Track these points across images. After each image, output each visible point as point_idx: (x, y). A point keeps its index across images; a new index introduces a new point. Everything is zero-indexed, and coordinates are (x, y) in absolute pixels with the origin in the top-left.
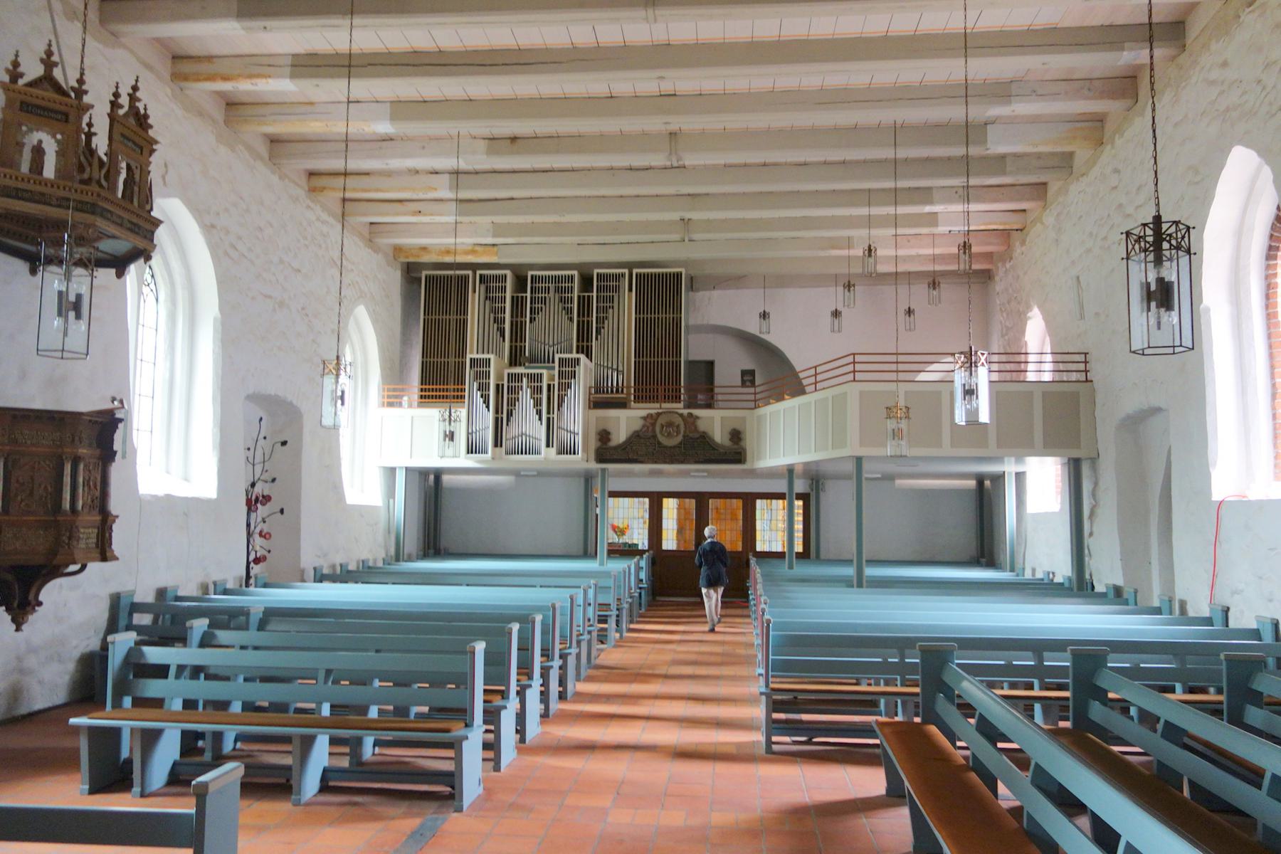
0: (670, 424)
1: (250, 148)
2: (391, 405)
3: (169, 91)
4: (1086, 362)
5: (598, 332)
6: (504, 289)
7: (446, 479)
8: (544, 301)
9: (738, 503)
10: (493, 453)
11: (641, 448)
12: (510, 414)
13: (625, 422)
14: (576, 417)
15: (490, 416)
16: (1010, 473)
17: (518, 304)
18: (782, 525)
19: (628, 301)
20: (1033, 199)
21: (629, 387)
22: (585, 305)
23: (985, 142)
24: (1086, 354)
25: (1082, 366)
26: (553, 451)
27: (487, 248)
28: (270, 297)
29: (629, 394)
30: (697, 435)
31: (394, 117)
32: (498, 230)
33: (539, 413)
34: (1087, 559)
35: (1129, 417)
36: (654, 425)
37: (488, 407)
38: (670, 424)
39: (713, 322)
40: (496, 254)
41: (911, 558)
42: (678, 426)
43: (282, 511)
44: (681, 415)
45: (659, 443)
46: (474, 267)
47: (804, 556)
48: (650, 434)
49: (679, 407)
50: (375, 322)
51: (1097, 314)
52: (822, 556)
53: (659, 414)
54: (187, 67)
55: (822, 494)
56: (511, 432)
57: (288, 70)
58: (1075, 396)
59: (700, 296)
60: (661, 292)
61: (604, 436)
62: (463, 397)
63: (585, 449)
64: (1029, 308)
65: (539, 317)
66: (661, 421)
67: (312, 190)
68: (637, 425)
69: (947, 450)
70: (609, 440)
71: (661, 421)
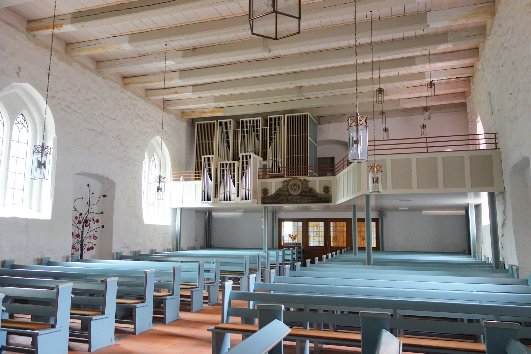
0: (295, 185)
1: (82, 65)
2: (174, 180)
3: (25, 37)
4: (496, 138)
6: (229, 128)
7: (214, 214)
8: (246, 132)
9: (322, 224)
10: (214, 200)
11: (282, 196)
13: (274, 185)
14: (250, 182)
16: (471, 205)
17: (236, 134)
18: (322, 234)
19: (283, 129)
20: (470, 57)
21: (284, 168)
22: (264, 131)
23: (426, 21)
24: (495, 134)
25: (493, 141)
27: (220, 109)
28: (93, 130)
29: (284, 172)
30: (307, 190)
31: (131, 41)
32: (217, 99)
33: (234, 181)
34: (501, 250)
35: (515, 167)
36: (287, 185)
37: (211, 179)
38: (295, 185)
39: (330, 138)
40: (223, 112)
41: (432, 251)
42: (299, 186)
43: (103, 227)
44: (300, 180)
45: (290, 194)
47: (376, 249)
48: (286, 190)
50: (168, 145)
51: (499, 110)
52: (385, 249)
53: (290, 180)
54: (33, 25)
55: (384, 219)
56: (221, 191)
57: (70, 20)
58: (490, 157)
59: (325, 126)
60: (298, 123)
61: (265, 191)
62: (200, 176)
63: (254, 197)
64: (477, 117)
65: (245, 139)
66: (291, 183)
67: (125, 84)
68: (280, 186)
69: (415, 190)
70: (267, 193)
71: (291, 183)
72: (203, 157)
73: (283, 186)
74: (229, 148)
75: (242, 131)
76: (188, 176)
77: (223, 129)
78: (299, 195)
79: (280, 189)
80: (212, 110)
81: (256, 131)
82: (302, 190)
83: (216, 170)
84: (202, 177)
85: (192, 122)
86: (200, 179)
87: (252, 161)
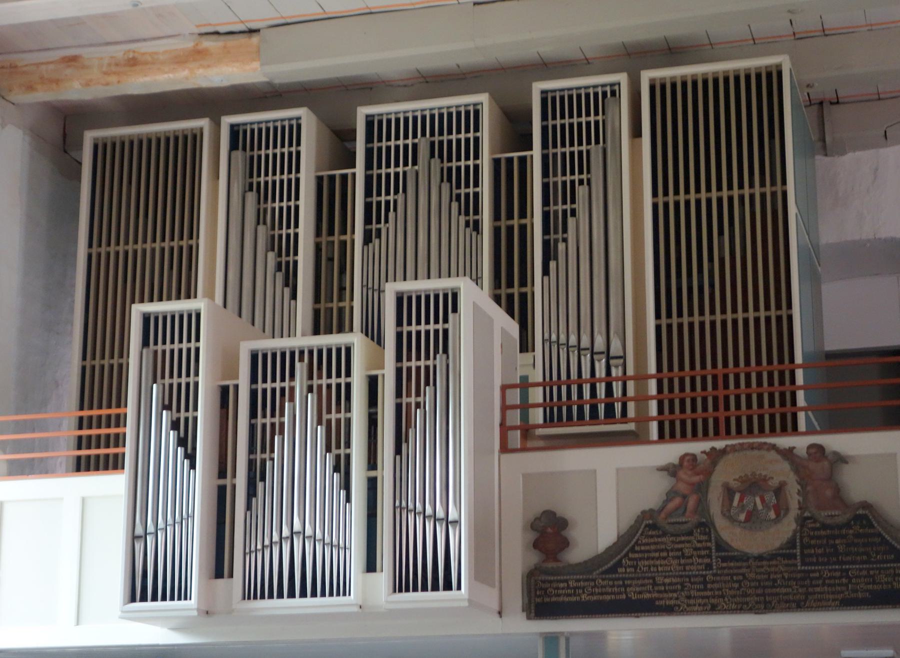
5: (549, 254)
12: (256, 474)
13: (613, 486)
15: (199, 484)
19: (632, 163)
22: (510, 180)
26: (383, 578)
27: (243, 40)
36: (702, 489)
38: (753, 485)
39: (887, 232)
42: (779, 491)
44: (788, 454)
45: (721, 546)
46: (211, 102)
48: (692, 519)
49: (799, 443)
53: (715, 456)
59: (851, 166)
63: (481, 574)
65: (388, 228)
66: (726, 474)
68: (651, 494)
71: (726, 474)
72: (138, 310)
73: (671, 495)
74: (290, 281)
75: (368, 180)
76: (29, 446)
77: (252, 168)
78: (786, 552)
79: (651, 510)
80: (190, 45)
81: (459, 180)
82: (802, 521)
83: (225, 396)
84: (128, 450)
85: (62, 130)
86: (114, 464)
87: (464, 327)
